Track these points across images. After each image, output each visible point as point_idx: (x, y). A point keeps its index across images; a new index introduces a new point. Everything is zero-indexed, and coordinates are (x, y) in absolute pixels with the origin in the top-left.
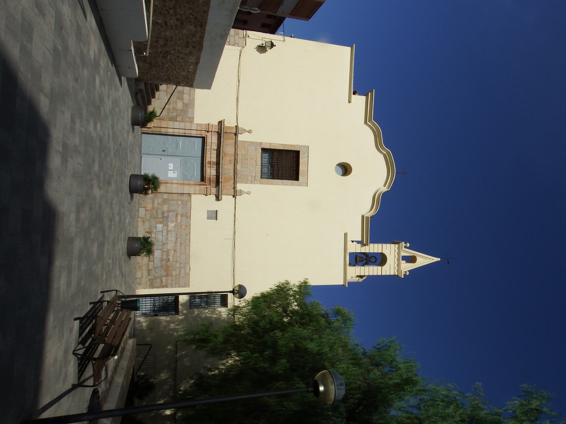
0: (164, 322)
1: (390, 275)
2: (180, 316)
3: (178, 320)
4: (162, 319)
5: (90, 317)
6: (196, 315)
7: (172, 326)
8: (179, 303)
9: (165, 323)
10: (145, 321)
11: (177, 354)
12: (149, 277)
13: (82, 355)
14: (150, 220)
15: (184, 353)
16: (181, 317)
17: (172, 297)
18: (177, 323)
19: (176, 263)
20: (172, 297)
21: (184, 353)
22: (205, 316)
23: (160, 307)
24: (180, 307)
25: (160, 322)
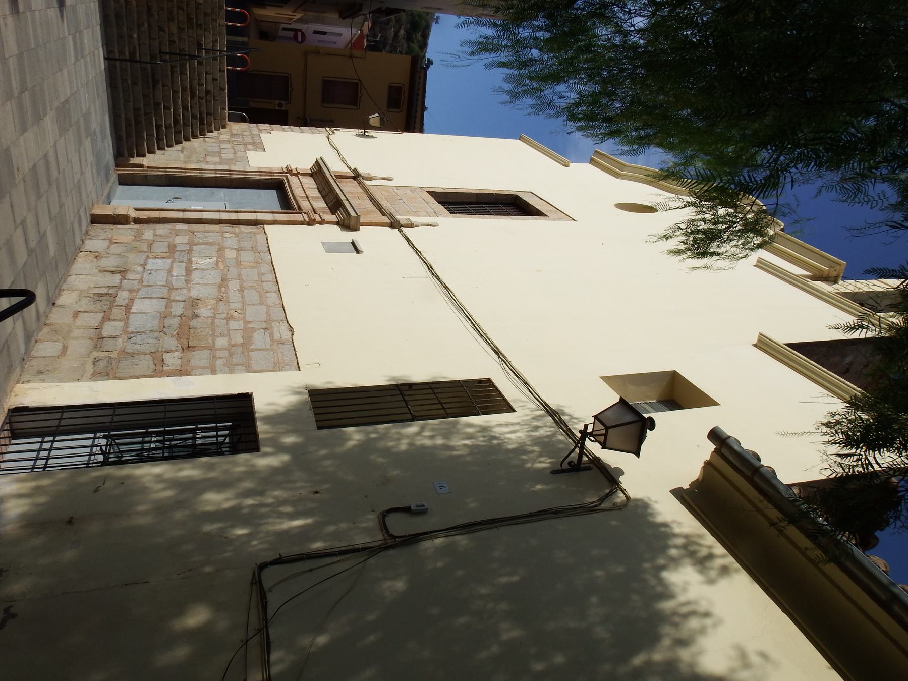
0: (160, 486)
1: (865, 338)
2: (266, 455)
3: (252, 473)
4: (142, 476)
5: (431, 388)
6: (354, 446)
7: (214, 500)
8: (257, 415)
9: (168, 493)
10: (23, 491)
11: (267, 647)
12: (95, 354)
13: (102, 461)
14: (126, 254)
15: (322, 640)
16: (265, 461)
17: (217, 436)
18: (248, 485)
19: (227, 321)
20: (217, 429)
21: (322, 640)
22: (411, 444)
23: (899, 326)
24: (261, 427)
25: (135, 490)
